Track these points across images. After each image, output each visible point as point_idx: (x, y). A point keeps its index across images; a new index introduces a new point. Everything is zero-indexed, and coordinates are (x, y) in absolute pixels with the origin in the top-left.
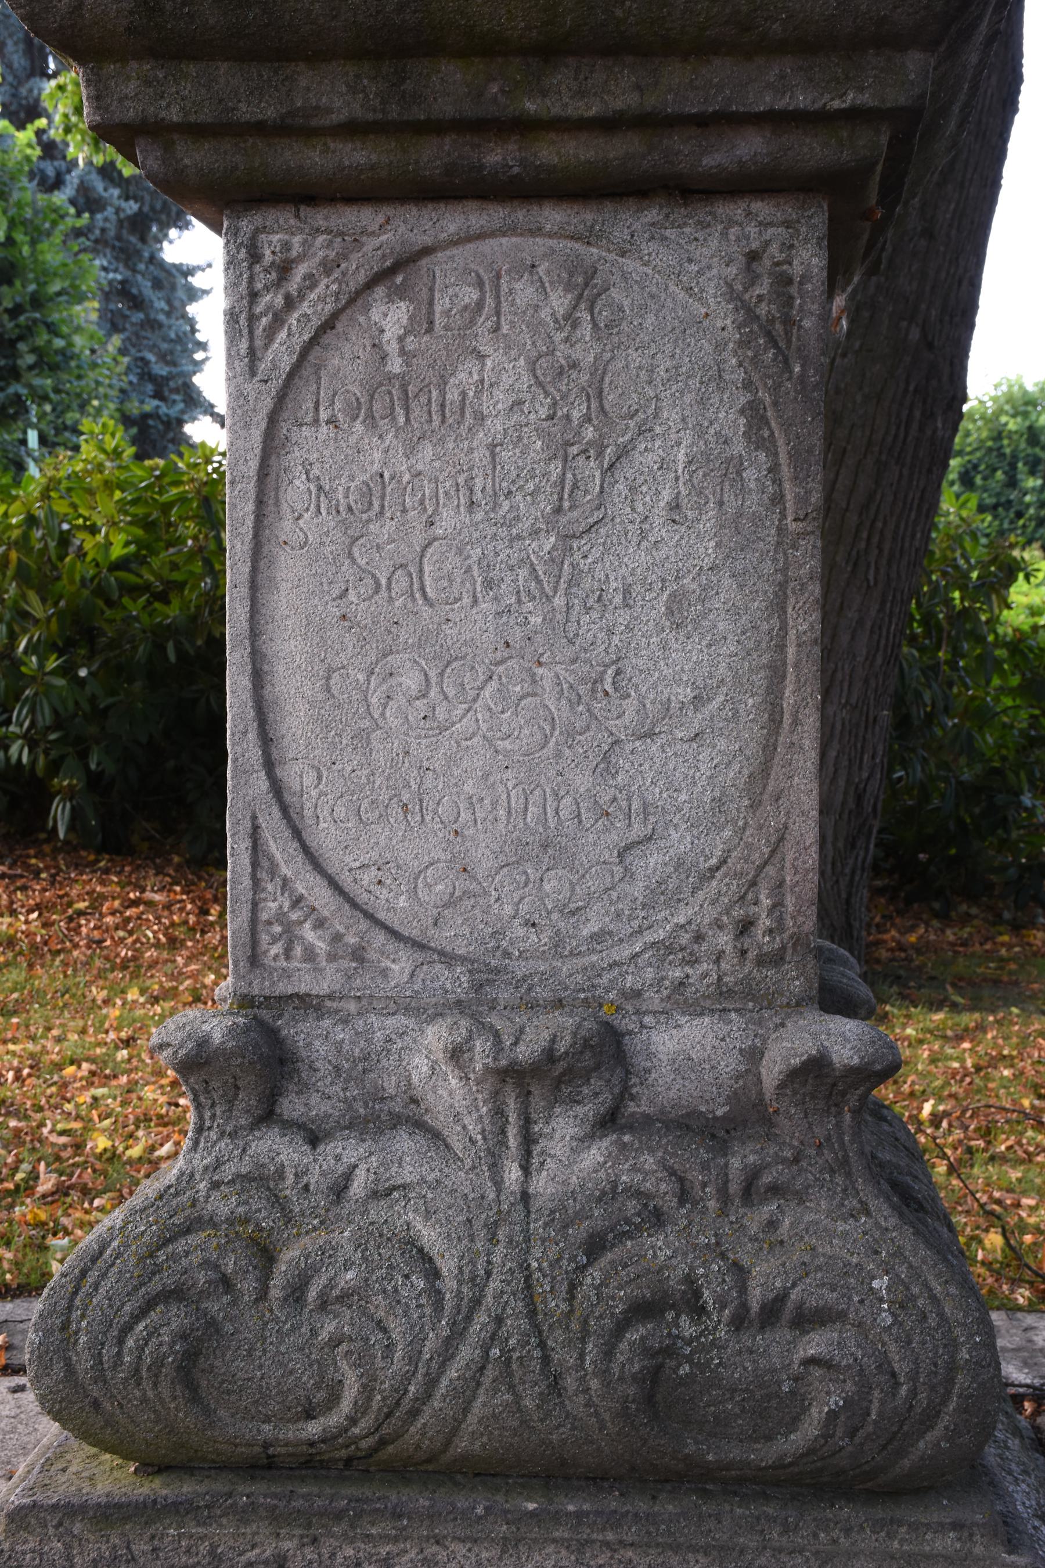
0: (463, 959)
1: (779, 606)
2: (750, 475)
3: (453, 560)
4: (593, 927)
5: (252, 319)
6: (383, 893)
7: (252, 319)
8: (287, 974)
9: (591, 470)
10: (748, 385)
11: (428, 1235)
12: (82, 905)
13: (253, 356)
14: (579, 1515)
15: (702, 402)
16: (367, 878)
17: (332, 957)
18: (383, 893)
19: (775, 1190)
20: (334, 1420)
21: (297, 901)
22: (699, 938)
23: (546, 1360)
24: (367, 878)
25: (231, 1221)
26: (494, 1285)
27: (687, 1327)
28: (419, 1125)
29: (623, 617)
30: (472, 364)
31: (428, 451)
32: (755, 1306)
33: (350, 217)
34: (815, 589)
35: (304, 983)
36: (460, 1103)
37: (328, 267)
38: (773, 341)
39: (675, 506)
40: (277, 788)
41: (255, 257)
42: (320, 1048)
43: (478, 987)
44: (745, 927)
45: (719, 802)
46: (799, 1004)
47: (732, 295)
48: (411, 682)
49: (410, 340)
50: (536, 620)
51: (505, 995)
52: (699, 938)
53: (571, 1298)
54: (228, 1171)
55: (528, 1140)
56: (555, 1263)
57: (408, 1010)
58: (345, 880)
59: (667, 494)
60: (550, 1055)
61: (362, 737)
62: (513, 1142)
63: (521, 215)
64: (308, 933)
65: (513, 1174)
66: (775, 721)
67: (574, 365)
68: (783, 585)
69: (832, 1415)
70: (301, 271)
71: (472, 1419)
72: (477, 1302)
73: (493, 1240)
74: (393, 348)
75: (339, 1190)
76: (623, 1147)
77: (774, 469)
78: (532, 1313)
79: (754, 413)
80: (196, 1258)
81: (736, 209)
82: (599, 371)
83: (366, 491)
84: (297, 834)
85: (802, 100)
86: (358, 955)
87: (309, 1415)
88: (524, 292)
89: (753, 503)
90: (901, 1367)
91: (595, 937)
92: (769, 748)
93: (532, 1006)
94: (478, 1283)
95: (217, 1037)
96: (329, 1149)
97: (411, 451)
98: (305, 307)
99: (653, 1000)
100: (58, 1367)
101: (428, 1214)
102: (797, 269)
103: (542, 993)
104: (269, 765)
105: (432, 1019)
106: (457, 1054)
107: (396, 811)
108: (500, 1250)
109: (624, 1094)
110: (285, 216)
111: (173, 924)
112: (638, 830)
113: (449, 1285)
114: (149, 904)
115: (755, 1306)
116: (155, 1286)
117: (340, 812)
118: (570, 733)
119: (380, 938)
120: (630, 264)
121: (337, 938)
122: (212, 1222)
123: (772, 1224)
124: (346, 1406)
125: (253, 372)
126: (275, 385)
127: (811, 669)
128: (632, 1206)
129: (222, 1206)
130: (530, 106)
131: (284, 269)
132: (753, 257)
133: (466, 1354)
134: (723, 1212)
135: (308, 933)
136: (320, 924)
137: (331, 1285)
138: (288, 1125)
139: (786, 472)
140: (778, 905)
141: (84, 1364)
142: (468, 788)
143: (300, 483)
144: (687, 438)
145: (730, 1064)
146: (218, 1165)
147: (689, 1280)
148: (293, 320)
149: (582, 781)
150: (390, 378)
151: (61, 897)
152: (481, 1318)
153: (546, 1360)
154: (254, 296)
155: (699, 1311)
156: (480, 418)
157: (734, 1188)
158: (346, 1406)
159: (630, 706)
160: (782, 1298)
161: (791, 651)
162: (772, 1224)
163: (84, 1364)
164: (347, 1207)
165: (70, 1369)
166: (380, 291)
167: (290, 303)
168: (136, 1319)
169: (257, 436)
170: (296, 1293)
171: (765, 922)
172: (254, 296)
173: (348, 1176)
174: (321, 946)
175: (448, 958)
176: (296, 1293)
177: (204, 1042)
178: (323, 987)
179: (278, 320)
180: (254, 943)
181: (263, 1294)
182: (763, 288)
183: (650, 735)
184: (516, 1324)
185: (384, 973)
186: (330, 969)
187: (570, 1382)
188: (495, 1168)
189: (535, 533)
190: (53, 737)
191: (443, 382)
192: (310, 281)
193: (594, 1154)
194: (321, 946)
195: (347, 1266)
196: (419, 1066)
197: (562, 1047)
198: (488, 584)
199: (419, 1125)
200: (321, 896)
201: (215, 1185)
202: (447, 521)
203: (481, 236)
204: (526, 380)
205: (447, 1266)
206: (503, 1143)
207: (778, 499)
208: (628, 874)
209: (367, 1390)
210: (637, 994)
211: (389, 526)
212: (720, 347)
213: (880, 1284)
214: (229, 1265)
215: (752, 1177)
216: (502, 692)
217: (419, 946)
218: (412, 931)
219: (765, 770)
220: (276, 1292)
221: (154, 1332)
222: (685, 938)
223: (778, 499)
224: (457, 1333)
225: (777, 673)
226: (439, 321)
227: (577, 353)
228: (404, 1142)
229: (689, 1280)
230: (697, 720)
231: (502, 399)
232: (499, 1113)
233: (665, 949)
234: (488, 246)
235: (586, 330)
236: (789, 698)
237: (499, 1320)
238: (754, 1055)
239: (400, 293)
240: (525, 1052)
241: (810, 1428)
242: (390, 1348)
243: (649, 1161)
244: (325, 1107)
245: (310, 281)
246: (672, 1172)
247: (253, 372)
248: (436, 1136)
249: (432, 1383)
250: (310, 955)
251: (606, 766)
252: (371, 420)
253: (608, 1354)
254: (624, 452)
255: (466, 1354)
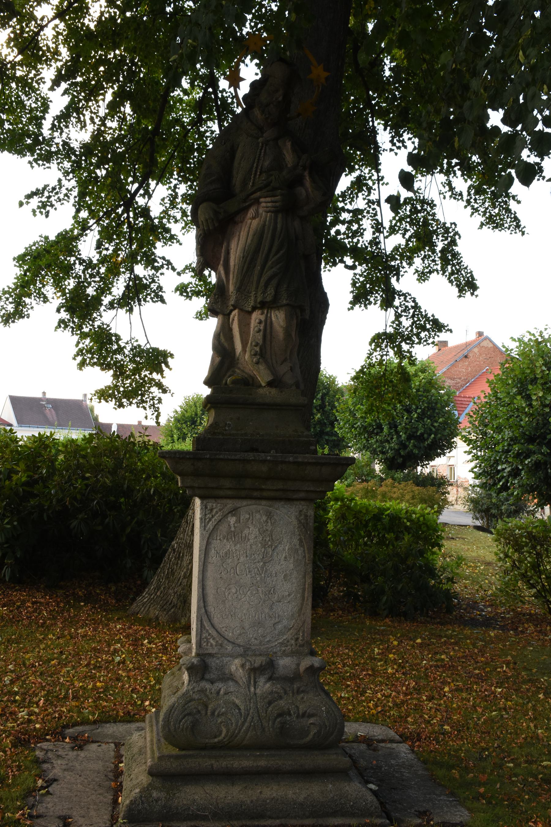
0: (242, 646)
1: (304, 577)
2: (300, 552)
3: (243, 567)
4: (268, 639)
5: (205, 519)
6: (227, 633)
7: (205, 519)
8: (207, 649)
9: (270, 550)
10: (299, 535)
11: (237, 701)
12: (19, 604)
13: (205, 526)
14: (267, 755)
15: (291, 538)
16: (223, 630)
17: (216, 646)
18: (227, 633)
19: (303, 691)
20: (220, 738)
21: (209, 634)
22: (288, 641)
23: (262, 725)
24: (223, 630)
25: (198, 699)
26: (251, 711)
27: (288, 718)
28: (233, 680)
29: (275, 579)
30: (247, 529)
31: (238, 546)
32: (301, 713)
33: (225, 501)
34: (311, 574)
35: (211, 651)
36: (242, 675)
37: (220, 510)
38: (304, 527)
39: (285, 558)
40: (206, 611)
41: (206, 508)
42: (213, 664)
43: (245, 651)
44: (297, 639)
45: (293, 615)
46: (306, 655)
47: (297, 518)
48: (234, 591)
49: (236, 525)
50: (258, 579)
51: (250, 653)
52: (288, 641)
53: (266, 713)
54: (196, 689)
55: (255, 682)
56: (263, 706)
57: (231, 656)
58: (219, 630)
59: (284, 555)
60: (261, 665)
61: (224, 602)
62: (252, 683)
63: (258, 502)
64: (211, 641)
65: (252, 689)
66: (303, 599)
67: (267, 530)
68: (305, 573)
69: (315, 734)
70: (215, 511)
71: (247, 737)
72: (248, 714)
73: (250, 702)
74: (232, 526)
75: (218, 693)
76: (274, 683)
77: (304, 551)
78: (259, 716)
79: (301, 540)
80: (193, 707)
81: (298, 503)
82: (272, 531)
83: (226, 553)
84: (210, 621)
85: (312, 489)
86: (221, 645)
87: (215, 737)
88: (258, 516)
89: (300, 558)
90: (327, 724)
91: (268, 641)
92: (302, 604)
93: (256, 655)
94: (248, 711)
95: (195, 662)
96: (216, 684)
97: (235, 545)
98: (215, 517)
99: (279, 654)
100: (167, 729)
101: (237, 698)
102: (309, 514)
103: (257, 653)
104: (205, 607)
105: (236, 658)
106: (243, 666)
107: (230, 616)
108: (252, 705)
109: (273, 673)
110: (213, 501)
111: (51, 610)
112: (277, 620)
113: (243, 711)
114: (40, 603)
115: (301, 713)
116: (186, 712)
117: (219, 616)
118: (264, 601)
119: (226, 642)
120: (278, 511)
121: (217, 642)
122: (194, 700)
123: (303, 698)
124: (223, 735)
125: (205, 529)
126: (209, 532)
127: (311, 590)
128: (276, 695)
129: (196, 696)
130: (263, 487)
131: (212, 510)
132: (301, 511)
133: (247, 724)
134: (293, 696)
135: (211, 641)
136: (214, 639)
137: (220, 712)
138: (207, 680)
139: (306, 551)
140: (303, 635)
141: (172, 728)
142: (244, 612)
143: (213, 551)
144: (288, 544)
145: (294, 666)
146: (194, 688)
147: (288, 709)
148: (213, 520)
149: (267, 610)
150: (232, 531)
151: (10, 601)
152: (249, 718)
153: (262, 725)
154: (206, 515)
155: (290, 715)
156: (249, 540)
157: (295, 691)
158: (223, 735)
159: (276, 596)
160: (306, 712)
161: (307, 586)
162: (303, 698)
163: (172, 728)
164: (220, 697)
165: (169, 729)
166: (230, 515)
167: (213, 517)
168: (182, 719)
169: (205, 542)
170: (213, 713)
171: (301, 638)
172: (206, 515)
173: (220, 690)
174: (214, 643)
175: (239, 646)
176: (213, 713)
177: (193, 663)
178: (214, 652)
179: (210, 520)
180: (200, 643)
181: (206, 714)
182: (302, 517)
183: (280, 602)
184: (256, 718)
185: (226, 649)
186: (216, 648)
187: (266, 729)
188: (249, 688)
189: (259, 562)
190: (5, 546)
191: (242, 532)
192: (217, 512)
193: (268, 685)
194: (214, 643)
195: (223, 708)
196: (233, 668)
197: (264, 664)
198: (249, 572)
199: (233, 680)
200: (214, 634)
201: (194, 692)
202: (242, 559)
203: (250, 505)
204: (258, 533)
205: (242, 708)
206: (250, 683)
207: (305, 557)
208: (275, 629)
209: (227, 732)
210: (276, 653)
211: (230, 560)
212: (294, 527)
213: (323, 709)
214: (200, 708)
215: (298, 689)
216: (251, 593)
217: (233, 643)
218: (232, 640)
219: (301, 609)
220: (209, 713)
221: (186, 721)
222: (285, 642)
223: (305, 557)
224: (245, 720)
225: (304, 590)
226: (241, 521)
227: (268, 528)
228: (231, 683)
229: (288, 709)
230: (289, 599)
231: (253, 536)
232: (249, 677)
233: (281, 644)
234: (251, 507)
235: (269, 524)
236: (306, 595)
237: (253, 718)
238: (298, 665)
239: (233, 515)
240: (256, 665)
241: (311, 736)
242: (232, 724)
243: (279, 686)
244: (214, 676)
245: (217, 512)
246: (283, 688)
247: (205, 529)
248: (236, 682)
249: (240, 730)
250: (212, 645)
251: (271, 608)
252: (228, 540)
253: (274, 723)
254: (276, 547)
255: (247, 724)
